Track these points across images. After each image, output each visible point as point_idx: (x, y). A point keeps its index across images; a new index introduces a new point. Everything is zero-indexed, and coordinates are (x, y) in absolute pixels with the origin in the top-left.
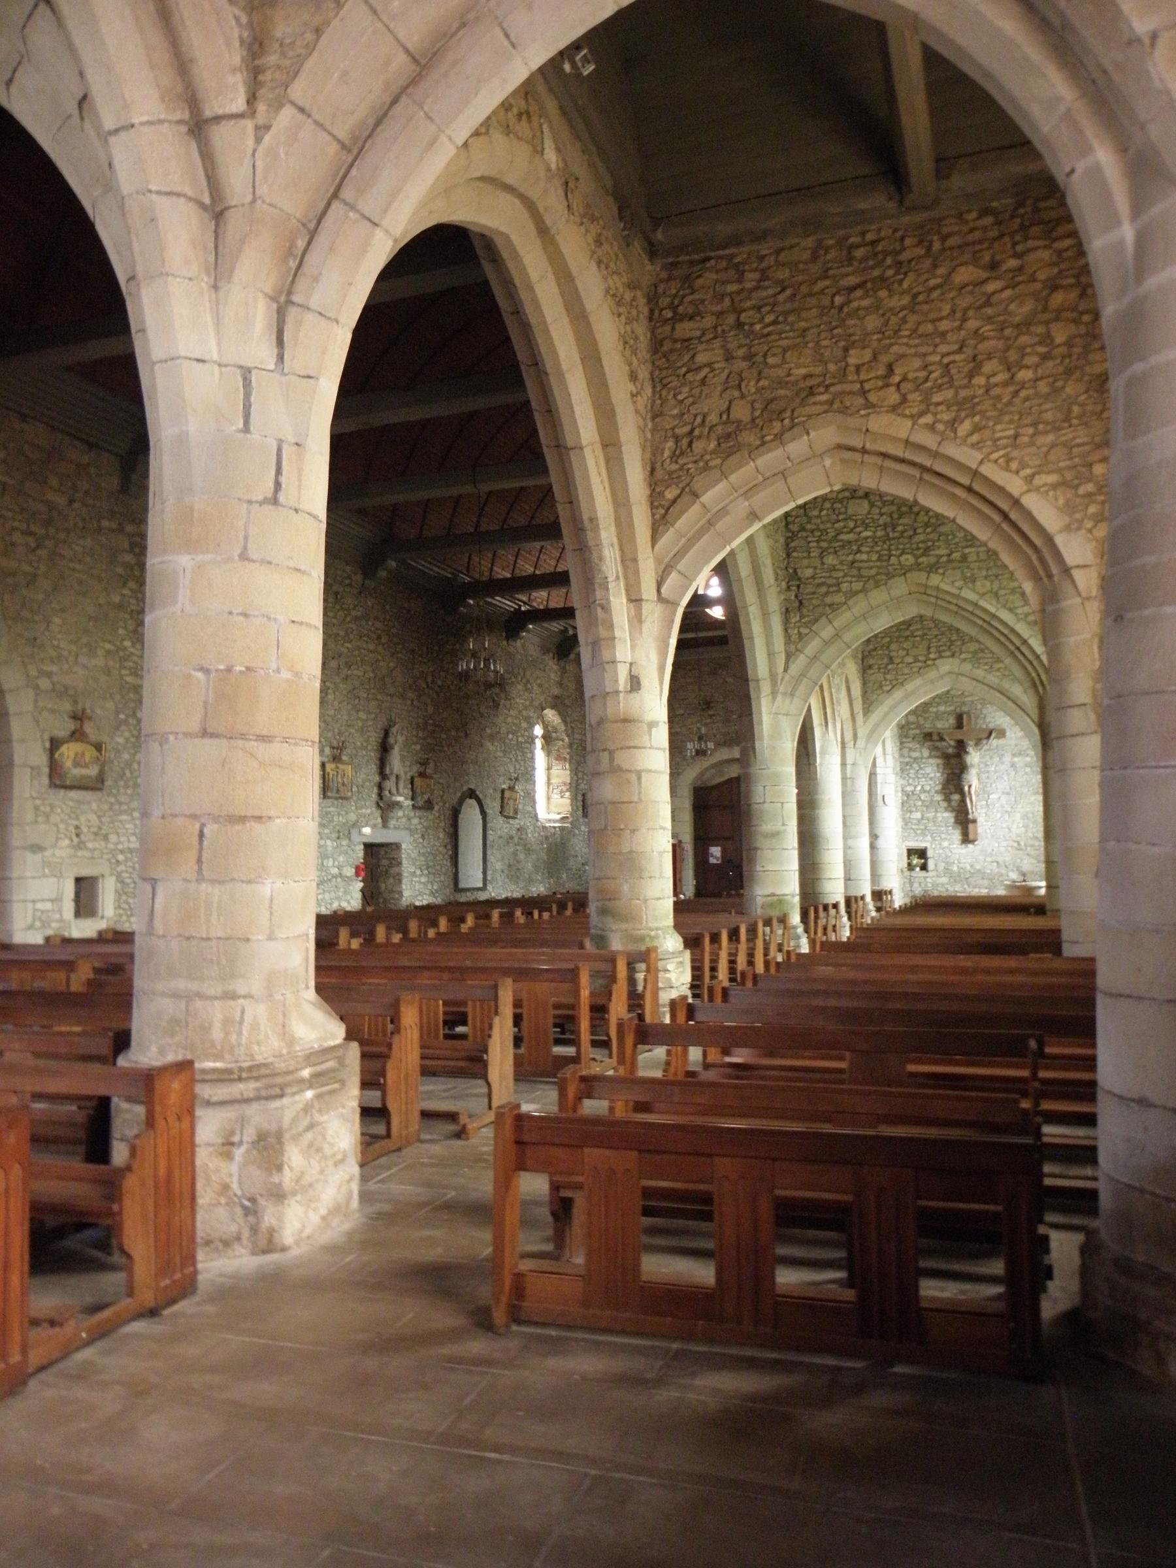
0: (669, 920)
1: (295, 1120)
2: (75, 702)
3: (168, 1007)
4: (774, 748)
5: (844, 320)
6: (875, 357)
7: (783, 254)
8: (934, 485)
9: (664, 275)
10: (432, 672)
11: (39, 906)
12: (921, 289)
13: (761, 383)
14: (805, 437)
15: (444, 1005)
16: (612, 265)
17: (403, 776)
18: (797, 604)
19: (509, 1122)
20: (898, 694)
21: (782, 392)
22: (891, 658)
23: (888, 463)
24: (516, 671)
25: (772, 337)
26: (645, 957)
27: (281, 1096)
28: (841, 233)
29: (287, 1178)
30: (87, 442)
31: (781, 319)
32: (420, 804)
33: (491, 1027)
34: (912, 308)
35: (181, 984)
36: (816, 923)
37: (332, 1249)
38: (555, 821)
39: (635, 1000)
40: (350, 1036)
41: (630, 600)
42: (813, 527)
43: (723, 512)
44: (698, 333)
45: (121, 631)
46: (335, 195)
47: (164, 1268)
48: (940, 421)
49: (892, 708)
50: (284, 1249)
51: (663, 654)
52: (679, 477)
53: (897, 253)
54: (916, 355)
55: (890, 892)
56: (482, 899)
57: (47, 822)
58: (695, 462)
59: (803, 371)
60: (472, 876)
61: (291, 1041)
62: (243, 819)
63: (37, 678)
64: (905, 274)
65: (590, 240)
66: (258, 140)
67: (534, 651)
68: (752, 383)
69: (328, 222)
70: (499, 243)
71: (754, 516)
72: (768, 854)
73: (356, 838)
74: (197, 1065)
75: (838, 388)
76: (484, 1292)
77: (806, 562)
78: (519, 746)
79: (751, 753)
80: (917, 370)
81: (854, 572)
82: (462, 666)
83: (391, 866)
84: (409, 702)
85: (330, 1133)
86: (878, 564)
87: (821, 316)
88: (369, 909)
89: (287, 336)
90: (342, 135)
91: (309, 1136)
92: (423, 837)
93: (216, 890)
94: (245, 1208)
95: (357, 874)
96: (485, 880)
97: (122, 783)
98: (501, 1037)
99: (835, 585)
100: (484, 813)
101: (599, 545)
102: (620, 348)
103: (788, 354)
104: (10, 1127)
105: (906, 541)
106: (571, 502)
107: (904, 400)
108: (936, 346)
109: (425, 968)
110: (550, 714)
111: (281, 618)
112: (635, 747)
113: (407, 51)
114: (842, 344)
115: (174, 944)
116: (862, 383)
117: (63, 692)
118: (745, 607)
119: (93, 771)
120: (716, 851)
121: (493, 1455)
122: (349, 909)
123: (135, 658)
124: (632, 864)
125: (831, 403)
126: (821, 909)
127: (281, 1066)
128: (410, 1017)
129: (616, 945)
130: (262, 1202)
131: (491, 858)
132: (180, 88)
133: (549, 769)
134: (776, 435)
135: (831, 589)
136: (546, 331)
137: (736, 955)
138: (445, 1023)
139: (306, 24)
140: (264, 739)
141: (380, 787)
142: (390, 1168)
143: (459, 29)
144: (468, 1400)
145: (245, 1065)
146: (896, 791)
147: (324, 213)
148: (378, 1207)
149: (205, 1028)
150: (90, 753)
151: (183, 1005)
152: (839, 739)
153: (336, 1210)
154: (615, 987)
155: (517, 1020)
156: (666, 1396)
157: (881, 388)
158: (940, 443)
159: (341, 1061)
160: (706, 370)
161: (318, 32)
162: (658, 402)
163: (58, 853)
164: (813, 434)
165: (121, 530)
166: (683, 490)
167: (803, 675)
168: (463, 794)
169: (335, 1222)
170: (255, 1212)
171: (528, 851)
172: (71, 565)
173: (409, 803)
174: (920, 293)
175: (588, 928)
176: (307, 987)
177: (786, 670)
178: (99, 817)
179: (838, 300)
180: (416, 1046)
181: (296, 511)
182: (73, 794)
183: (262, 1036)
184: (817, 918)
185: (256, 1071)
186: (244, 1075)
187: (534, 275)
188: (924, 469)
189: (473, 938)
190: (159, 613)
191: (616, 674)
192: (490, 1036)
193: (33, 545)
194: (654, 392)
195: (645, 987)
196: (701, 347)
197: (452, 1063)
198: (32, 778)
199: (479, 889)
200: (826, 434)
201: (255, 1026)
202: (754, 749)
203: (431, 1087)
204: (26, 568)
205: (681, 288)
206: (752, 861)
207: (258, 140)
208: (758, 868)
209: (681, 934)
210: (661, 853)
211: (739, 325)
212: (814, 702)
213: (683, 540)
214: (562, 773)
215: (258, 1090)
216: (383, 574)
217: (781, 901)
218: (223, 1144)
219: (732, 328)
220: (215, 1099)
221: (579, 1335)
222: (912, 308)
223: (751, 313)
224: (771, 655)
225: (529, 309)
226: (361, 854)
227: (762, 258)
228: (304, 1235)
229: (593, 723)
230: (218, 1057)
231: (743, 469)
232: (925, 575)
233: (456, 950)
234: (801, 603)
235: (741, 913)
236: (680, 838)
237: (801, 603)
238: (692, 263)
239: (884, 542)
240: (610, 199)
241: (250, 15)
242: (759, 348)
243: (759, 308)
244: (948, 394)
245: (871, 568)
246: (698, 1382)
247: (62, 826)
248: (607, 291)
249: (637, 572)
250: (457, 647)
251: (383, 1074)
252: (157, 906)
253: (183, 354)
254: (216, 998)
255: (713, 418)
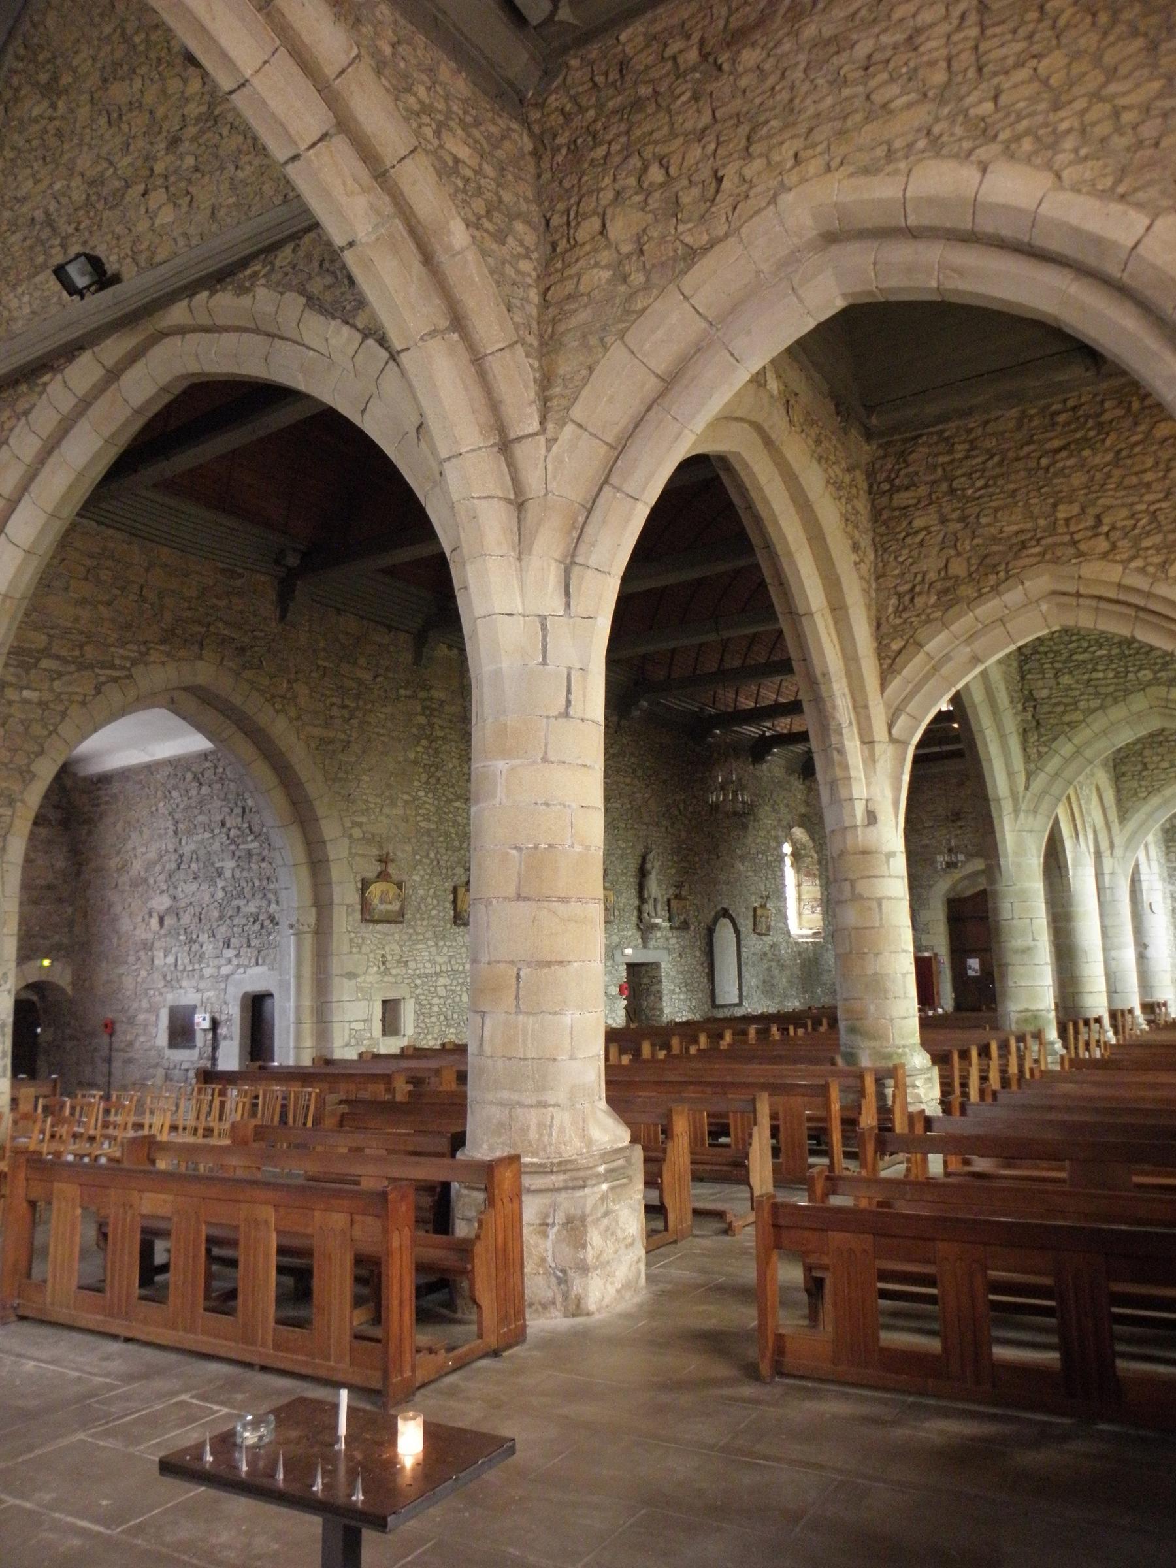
0: (916, 1039)
1: (595, 1207)
2: (381, 848)
3: (497, 1114)
4: (1019, 865)
5: (1051, 479)
6: (1083, 510)
7: (988, 426)
8: (1148, 622)
9: (880, 453)
10: (684, 801)
11: (353, 1025)
12: (1123, 445)
13: (976, 541)
14: (1020, 587)
15: (708, 1116)
16: (832, 458)
17: (660, 898)
18: (1034, 723)
19: (767, 1208)
20: (1155, 800)
21: (995, 548)
22: (1145, 764)
23: (1103, 605)
24: (763, 793)
25: (985, 500)
26: (891, 1073)
27: (584, 1187)
28: (1043, 402)
29: (590, 1255)
30: (385, 625)
31: (991, 482)
32: (677, 924)
33: (751, 1136)
34: (1117, 462)
35: (505, 1095)
36: (1076, 1039)
37: (627, 1316)
38: (807, 937)
39: (885, 1112)
40: (634, 1140)
41: (863, 743)
42: (1046, 649)
43: (947, 658)
44: (914, 501)
45: (416, 784)
46: (606, 481)
47: (504, 1319)
48: (1151, 564)
49: (1150, 815)
50: (588, 1314)
51: (898, 790)
52: (903, 630)
53: (1098, 415)
54: (1123, 505)
55: (1165, 1004)
56: (738, 1014)
57: (359, 952)
58: (918, 616)
59: (1015, 528)
60: (728, 992)
61: (589, 1143)
62: (549, 964)
63: (351, 828)
64: (1107, 434)
65: (810, 442)
66: (548, 450)
67: (779, 772)
68: (967, 542)
69: (601, 501)
70: (732, 460)
71: (976, 660)
72: (1020, 970)
73: (618, 958)
74: (526, 1160)
75: (1049, 541)
76: (752, 1353)
77: (1040, 683)
78: (769, 865)
79: (997, 871)
80: (1123, 520)
81: (1091, 690)
82: (713, 798)
83: (652, 984)
84: (663, 829)
85: (622, 1220)
86: (1115, 681)
87: (1030, 476)
88: (633, 1026)
89: (572, 589)
90: (610, 440)
91: (605, 1221)
92: (680, 956)
93: (531, 1020)
94: (558, 1278)
95: (621, 993)
96: (741, 996)
97: (418, 916)
98: (760, 1143)
99: (1071, 704)
100: (737, 932)
101: (832, 696)
102: (843, 526)
103: (999, 514)
104: (402, 1200)
105: (1142, 657)
106: (804, 660)
107: (1114, 547)
108: (1142, 496)
109: (691, 1083)
110: (798, 833)
111: (574, 805)
112: (874, 877)
113: (657, 376)
114: (1051, 500)
115: (500, 1063)
116: (1072, 534)
117: (370, 839)
118: (981, 731)
119: (395, 906)
120: (974, 964)
121: (762, 1462)
122: (614, 1025)
123: (427, 806)
124: (878, 986)
125: (1043, 554)
126: (1081, 1024)
127: (582, 1162)
128: (681, 1126)
129: (865, 1062)
130: (571, 1273)
131: (746, 975)
132: (492, 421)
133: (799, 885)
134: (992, 587)
135: (1068, 708)
136: (776, 522)
137: (988, 1071)
138: (710, 1133)
139: (581, 364)
140: (562, 900)
141: (640, 910)
142: (669, 1257)
143: (695, 353)
144: (742, 1426)
145: (555, 1161)
146: (1165, 898)
147: (597, 495)
148: (661, 1286)
149: (524, 1131)
150: (393, 890)
151: (507, 1111)
152: (1092, 850)
153: (628, 1285)
154: (864, 1102)
155: (775, 1132)
156: (900, 1433)
157: (1091, 538)
158: (1152, 584)
159: (628, 1160)
160: (924, 533)
161: (591, 369)
162: (880, 565)
163: (369, 979)
164: (1027, 584)
165: (414, 697)
166: (907, 642)
167: (1045, 792)
168: (717, 913)
169: (628, 1295)
170: (566, 1281)
171: (782, 967)
172: (377, 730)
173: (666, 924)
174: (1121, 450)
175: (838, 1045)
176: (600, 1099)
177: (1027, 788)
178: (401, 947)
179: (1044, 462)
180: (687, 1150)
181: (583, 720)
182: (379, 927)
183: (567, 1138)
184: (1077, 1032)
185: (563, 1166)
186: (555, 1169)
187: (763, 479)
188: (1138, 608)
189: (732, 1054)
190: (482, 805)
191: (853, 809)
192: (750, 1144)
193: (347, 716)
194: (876, 557)
195: (894, 1102)
196: (917, 514)
197: (718, 1168)
198: (348, 915)
199: (735, 1005)
200: (1040, 582)
201: (562, 1130)
202: (999, 866)
203: (698, 1191)
204: (343, 737)
205: (898, 463)
206: (1003, 976)
207: (548, 450)
208: (1011, 984)
209: (927, 1051)
210: (904, 975)
211: (952, 491)
212: (1062, 812)
213: (910, 686)
214: (812, 889)
215: (565, 1181)
216: (636, 713)
217: (1035, 1016)
218: (541, 1225)
219: (945, 494)
220: (533, 1188)
221: (828, 1387)
222: (1117, 462)
223: (963, 479)
224: (1010, 774)
225: (760, 506)
226: (624, 974)
227: (970, 431)
228: (605, 1303)
229: (834, 855)
230: (535, 1154)
231: (963, 620)
232: (1165, 689)
233: (717, 1066)
234: (1038, 723)
235: (995, 1027)
236: (936, 950)
237: (1038, 723)
238: (906, 441)
239: (1121, 660)
240: (827, 400)
241: (540, 360)
242: (972, 510)
243: (969, 475)
244: (1157, 539)
245: (1108, 685)
246: (927, 1425)
247: (371, 955)
248: (828, 482)
249: (868, 717)
250: (707, 774)
251: (660, 1175)
252: (486, 1033)
253: (497, 611)
254: (532, 1106)
255: (932, 576)
